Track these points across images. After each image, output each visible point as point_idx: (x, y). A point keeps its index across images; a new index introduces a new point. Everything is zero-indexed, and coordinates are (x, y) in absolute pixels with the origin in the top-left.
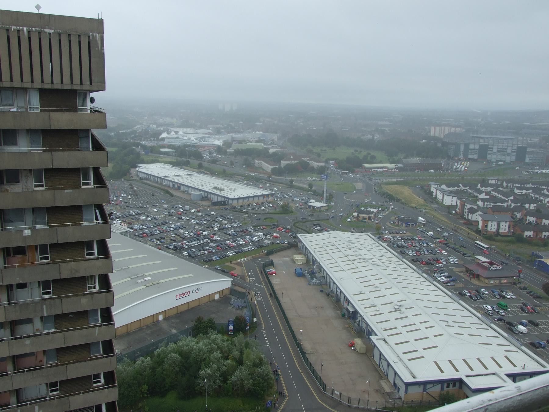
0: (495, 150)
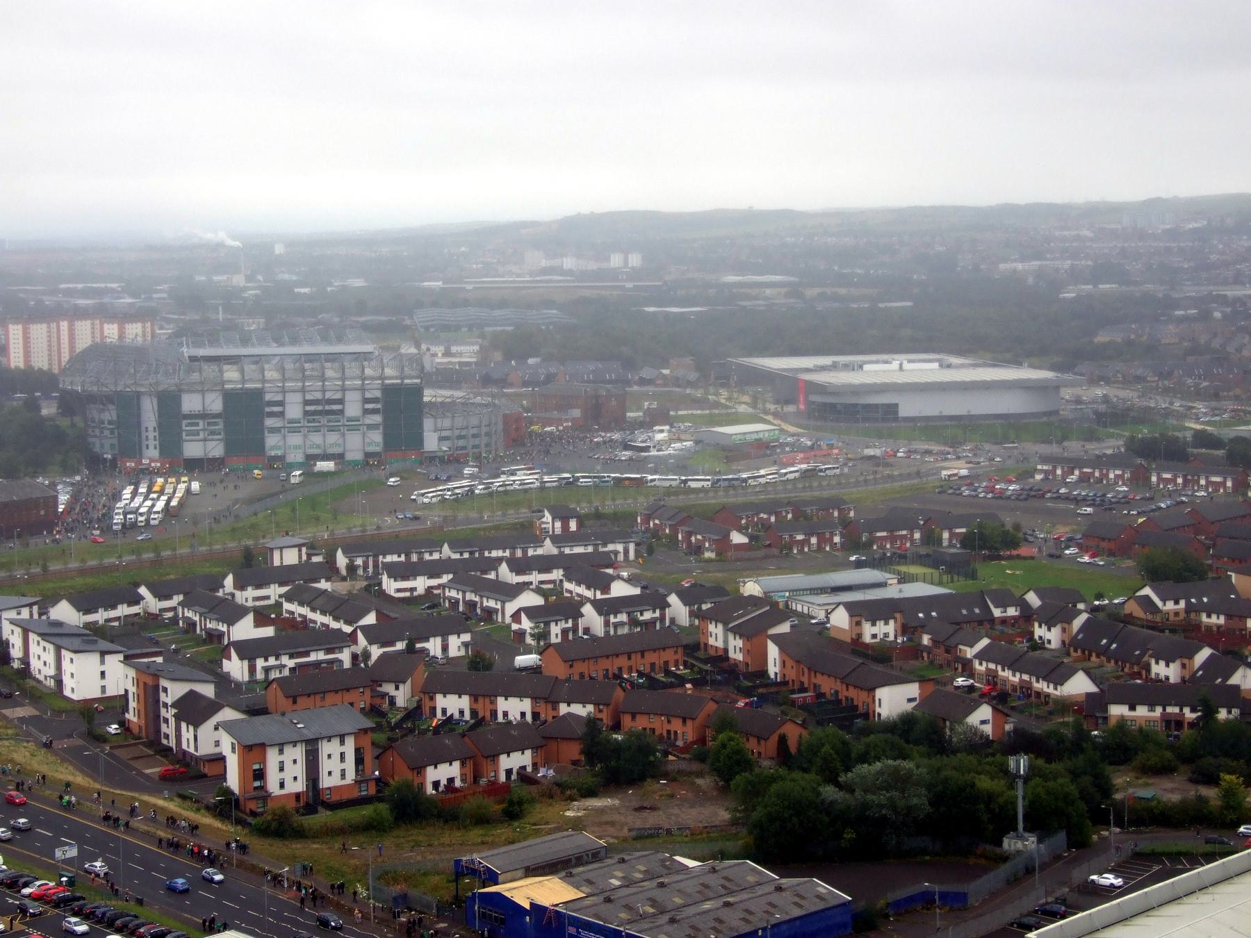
0: (294, 411)
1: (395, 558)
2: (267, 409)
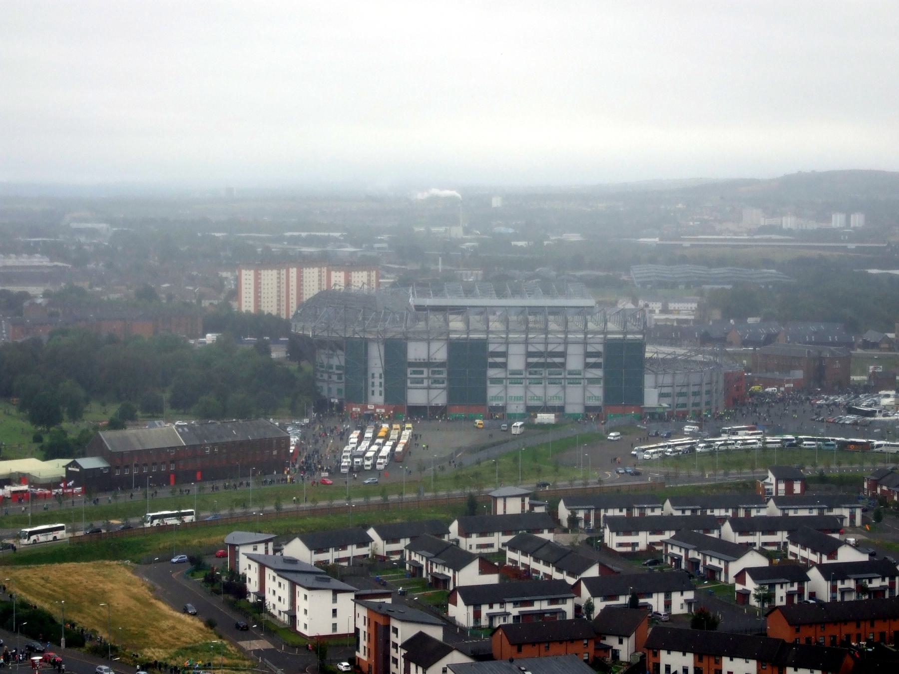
0: (516, 362)
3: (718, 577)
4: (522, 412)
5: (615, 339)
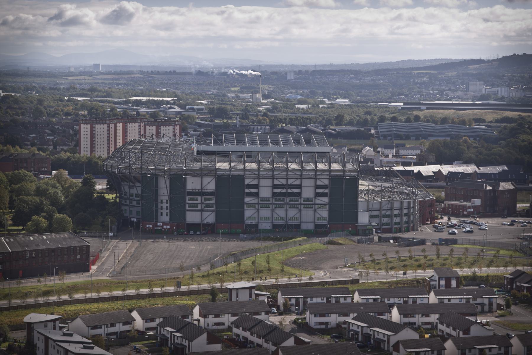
0: (265, 192)
1: (319, 300)
2: (247, 190)
3: (382, 346)
4: (269, 228)
5: (337, 176)
